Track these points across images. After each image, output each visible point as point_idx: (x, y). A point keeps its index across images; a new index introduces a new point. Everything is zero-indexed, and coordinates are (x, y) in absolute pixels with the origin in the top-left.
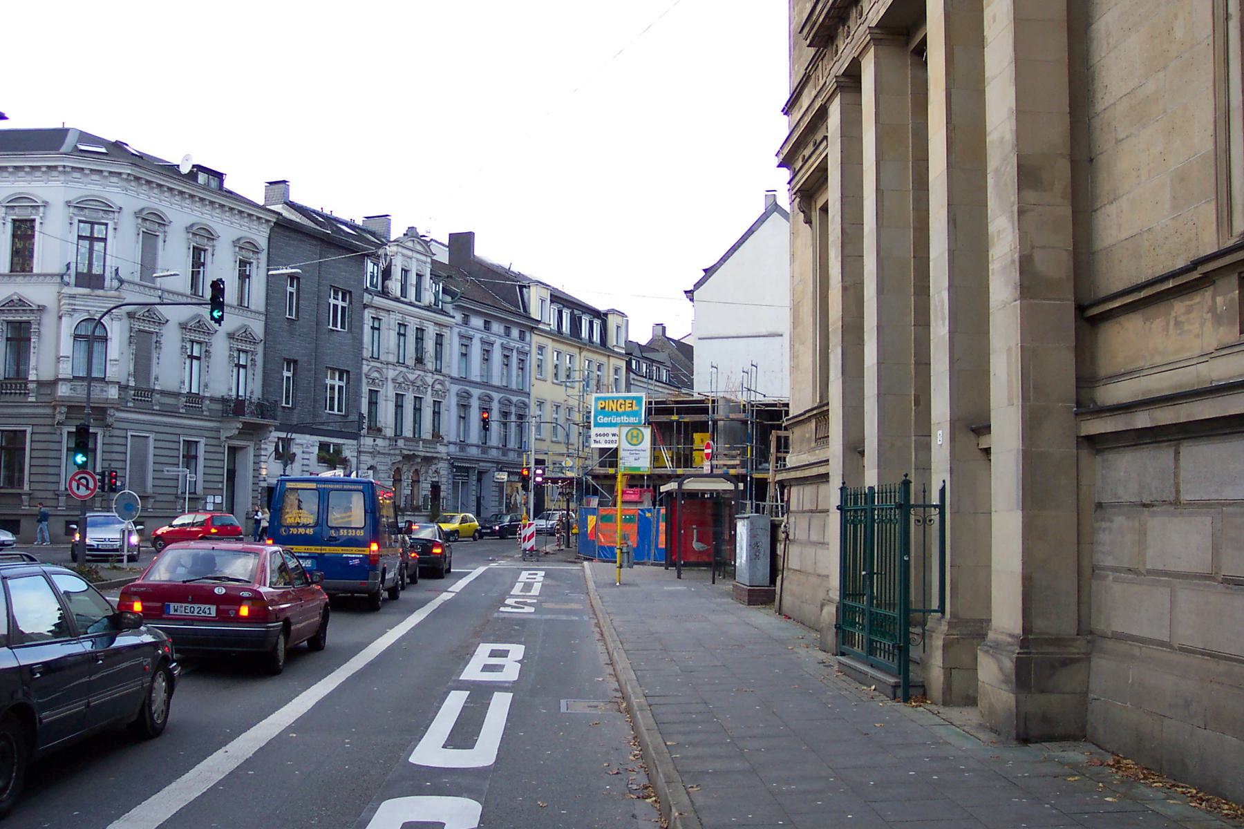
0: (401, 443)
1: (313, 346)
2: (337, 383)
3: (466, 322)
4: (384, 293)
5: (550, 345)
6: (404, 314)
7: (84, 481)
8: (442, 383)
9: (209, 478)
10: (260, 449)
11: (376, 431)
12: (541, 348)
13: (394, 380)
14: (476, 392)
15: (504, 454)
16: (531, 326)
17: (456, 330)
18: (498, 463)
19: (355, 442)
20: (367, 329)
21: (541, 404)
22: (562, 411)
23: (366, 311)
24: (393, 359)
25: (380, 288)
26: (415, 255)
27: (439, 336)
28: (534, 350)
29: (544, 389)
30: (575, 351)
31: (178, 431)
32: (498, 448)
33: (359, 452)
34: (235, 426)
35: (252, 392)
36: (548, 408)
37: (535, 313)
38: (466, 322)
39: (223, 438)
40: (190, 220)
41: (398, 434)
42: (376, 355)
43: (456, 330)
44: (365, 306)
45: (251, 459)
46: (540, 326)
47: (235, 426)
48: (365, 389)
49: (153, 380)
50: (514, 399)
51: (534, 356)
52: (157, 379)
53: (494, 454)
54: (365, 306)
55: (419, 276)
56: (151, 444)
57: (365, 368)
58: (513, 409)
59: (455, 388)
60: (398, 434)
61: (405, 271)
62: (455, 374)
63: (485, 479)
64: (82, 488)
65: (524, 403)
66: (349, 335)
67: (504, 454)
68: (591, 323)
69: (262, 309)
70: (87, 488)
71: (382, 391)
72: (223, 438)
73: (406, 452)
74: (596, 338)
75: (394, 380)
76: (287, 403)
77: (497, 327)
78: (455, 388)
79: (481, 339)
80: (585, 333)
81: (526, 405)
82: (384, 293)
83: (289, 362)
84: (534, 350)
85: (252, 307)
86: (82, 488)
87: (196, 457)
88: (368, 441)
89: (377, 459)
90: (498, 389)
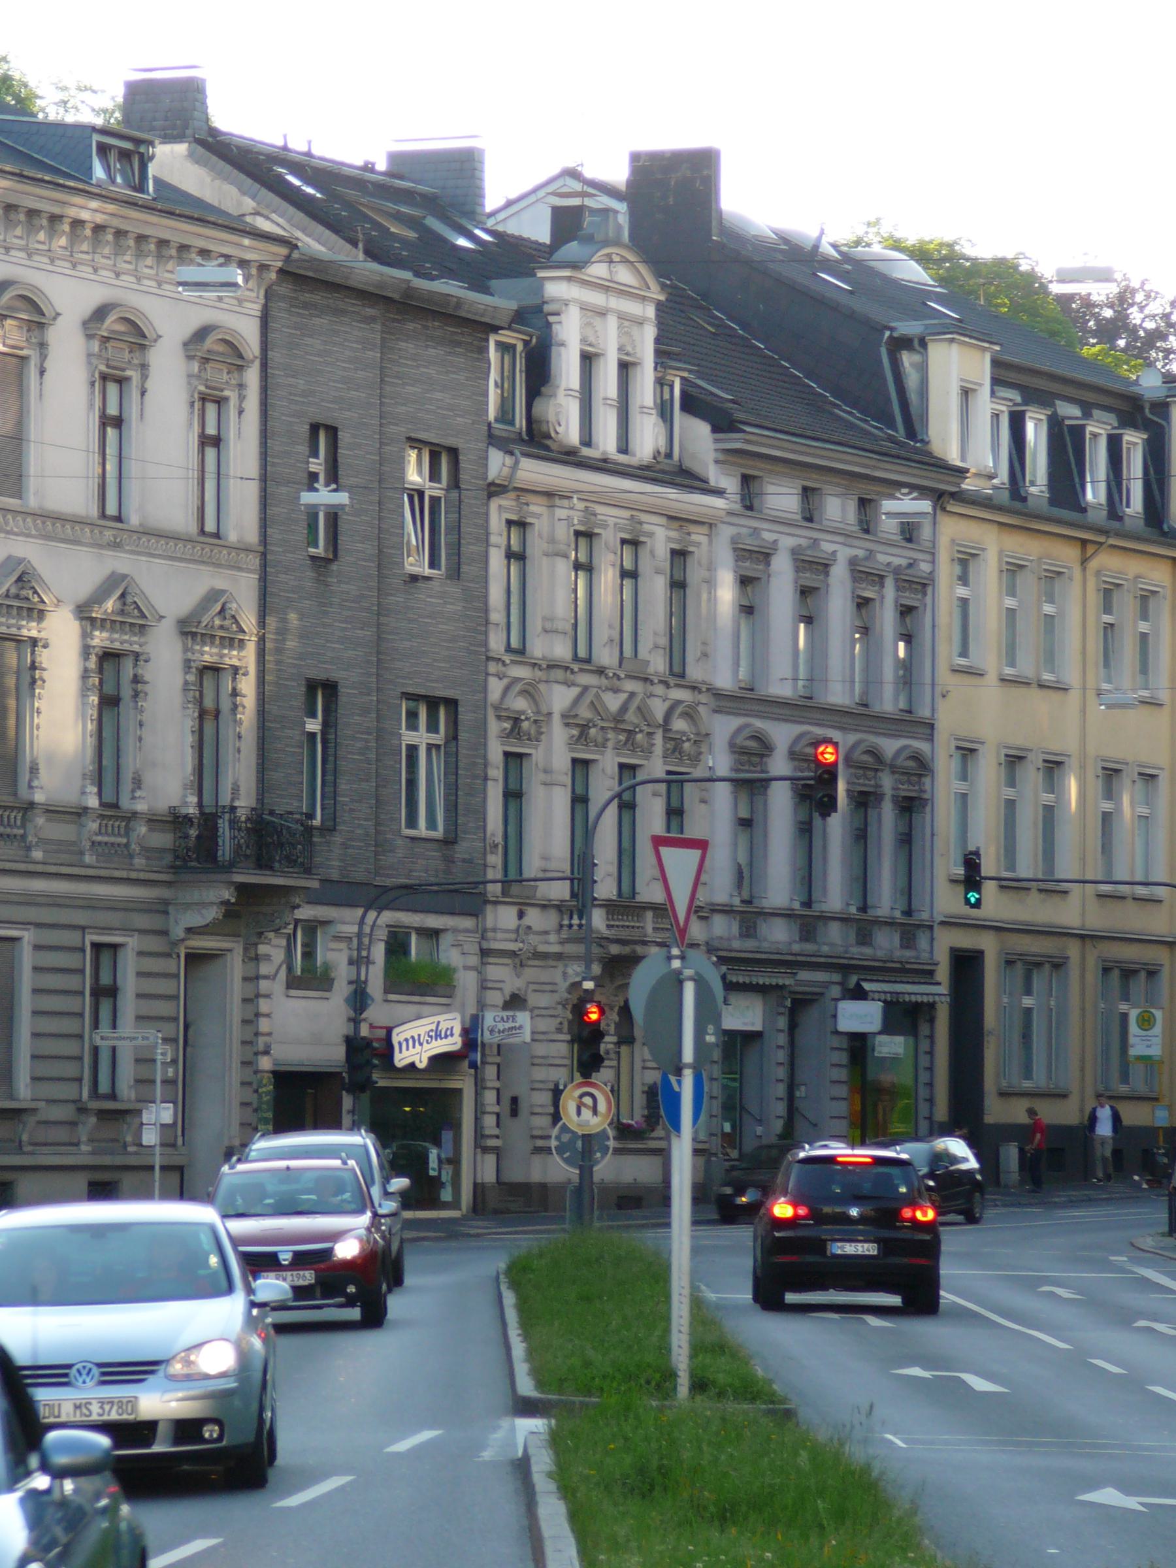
0: (598, 920)
1: (369, 633)
2: (421, 737)
3: (749, 501)
4: (536, 440)
5: (994, 545)
6: (592, 498)
7: (588, 1100)
8: (690, 714)
9: (51, 1047)
10: (257, 958)
11: (515, 882)
12: (966, 561)
13: (568, 718)
14: (782, 734)
15: (864, 938)
16: (945, 487)
17: (726, 533)
18: (845, 969)
19: (467, 923)
20: (496, 560)
21: (967, 752)
22: (1031, 775)
23: (494, 504)
24: (561, 650)
25: (520, 422)
26: (615, 303)
27: (679, 555)
28: (946, 571)
29: (975, 709)
30: (1068, 554)
31: (80, 918)
32: (845, 920)
33: (485, 953)
34: (208, 899)
35: (236, 790)
36: (988, 768)
37: (945, 440)
38: (749, 501)
39: (178, 932)
40: (95, 295)
41: (582, 896)
42: (582, 653)
43: (726, 533)
44: (495, 490)
45: (237, 989)
46: (968, 485)
47: (208, 899)
48: (495, 751)
49: (127, 785)
50: (890, 746)
51: (947, 590)
52: (138, 783)
53: (835, 938)
54: (495, 490)
55: (625, 367)
56: (27, 958)
57: (495, 688)
58: (887, 782)
59: (723, 728)
60: (582, 896)
61: (588, 359)
62: (724, 680)
63: (811, 1018)
64: (587, 1114)
65: (917, 757)
66: (454, 589)
67: (864, 938)
68: (1114, 443)
69: (252, 536)
70: (595, 1111)
71: (538, 755)
72: (178, 932)
73: (615, 949)
74: (1136, 504)
75: (568, 718)
76: (432, 824)
77: (782, 498)
78: (723, 728)
79: (795, 552)
80: (1094, 494)
81: (922, 767)
82: (536, 440)
83: (433, 703)
84: (946, 571)
85: (232, 537)
86: (587, 1114)
87: (112, 992)
88: (504, 917)
89: (530, 973)
90: (726, 702)
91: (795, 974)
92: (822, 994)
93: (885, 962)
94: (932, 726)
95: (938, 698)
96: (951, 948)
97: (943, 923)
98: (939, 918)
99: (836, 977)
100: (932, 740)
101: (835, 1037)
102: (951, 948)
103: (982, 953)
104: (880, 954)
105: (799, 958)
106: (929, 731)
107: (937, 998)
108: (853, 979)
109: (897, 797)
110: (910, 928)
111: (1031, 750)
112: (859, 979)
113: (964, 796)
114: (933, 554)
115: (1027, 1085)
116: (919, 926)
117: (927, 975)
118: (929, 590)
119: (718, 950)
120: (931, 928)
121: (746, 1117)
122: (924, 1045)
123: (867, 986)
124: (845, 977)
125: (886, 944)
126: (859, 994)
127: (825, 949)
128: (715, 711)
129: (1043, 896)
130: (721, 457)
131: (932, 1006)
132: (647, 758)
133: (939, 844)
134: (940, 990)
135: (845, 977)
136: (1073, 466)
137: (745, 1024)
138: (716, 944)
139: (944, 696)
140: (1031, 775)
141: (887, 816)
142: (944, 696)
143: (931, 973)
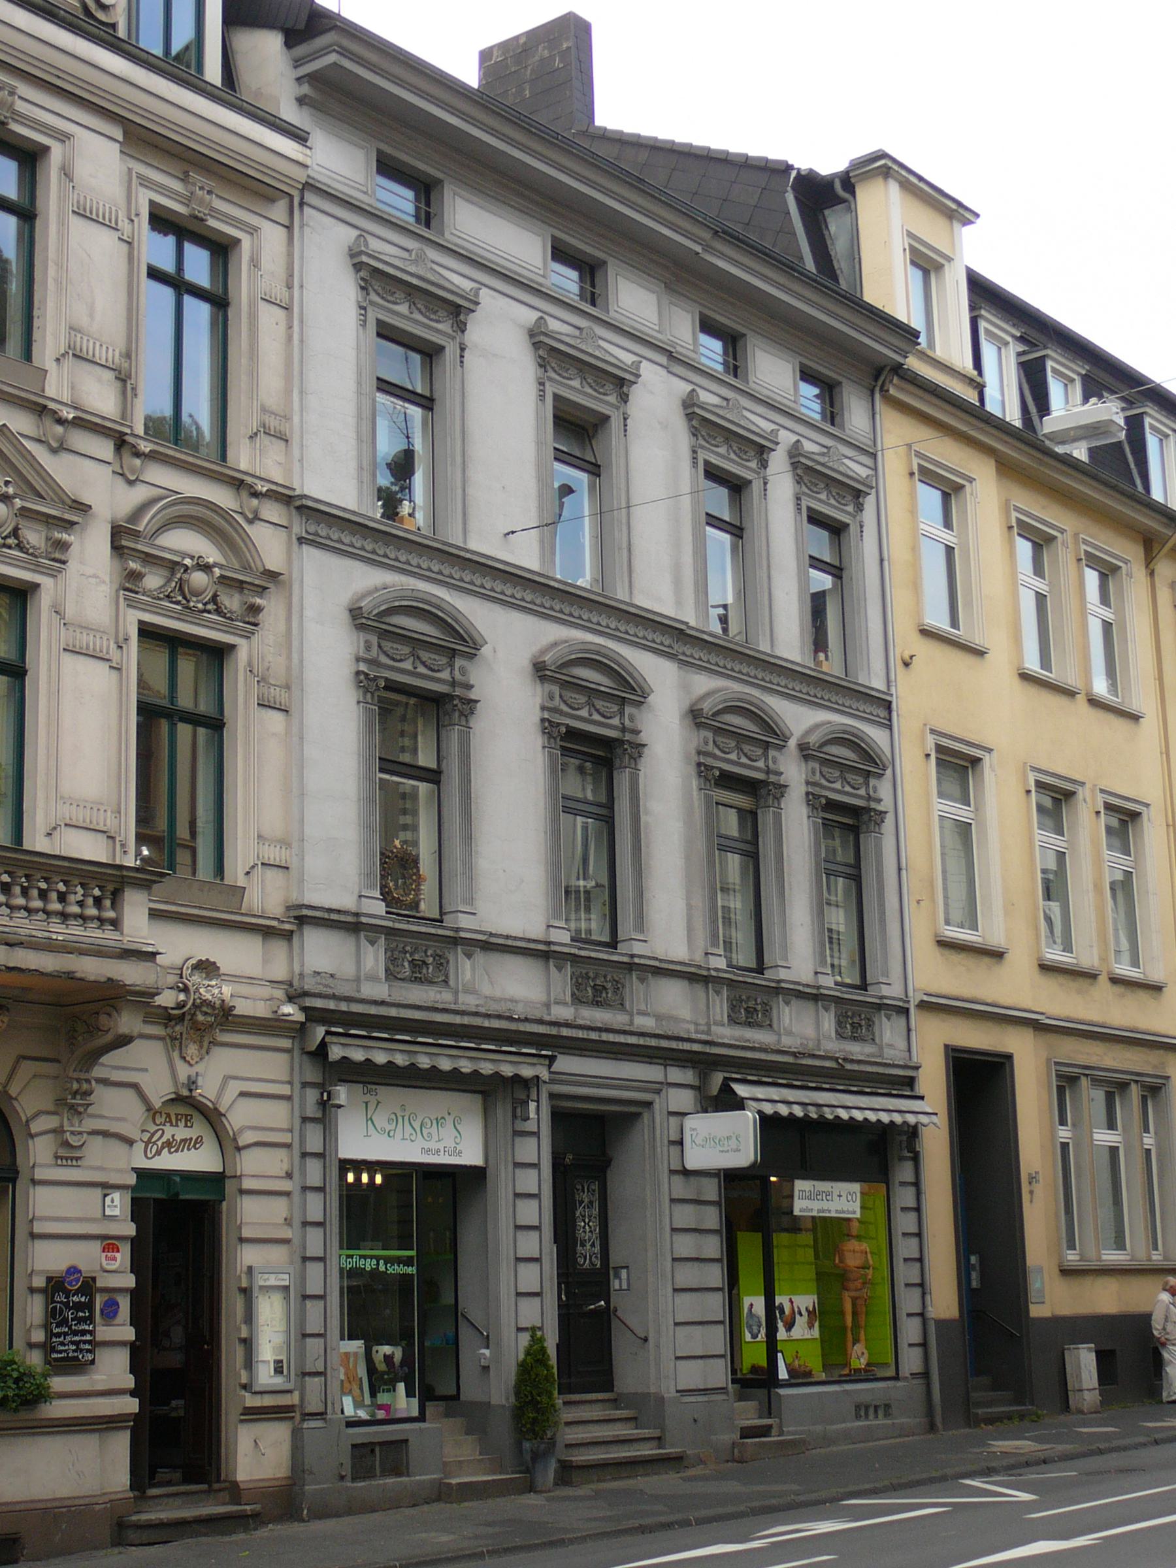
21: (958, 764)
22: (1088, 824)
91: (552, 1059)
92: (649, 1104)
93: (794, 1054)
94: (888, 706)
95: (899, 671)
96: (946, 1046)
97: (923, 1005)
98: (915, 998)
99: (687, 1076)
100: (890, 727)
101: (678, 1180)
102: (946, 1046)
103: (1009, 1057)
104: (787, 1042)
105: (565, 1032)
106: (883, 713)
107: (924, 1119)
108: (717, 1078)
109: (817, 797)
110: (858, 1010)
111: (1083, 784)
112: (725, 1078)
113: (964, 830)
114: (874, 456)
115: (1112, 1257)
116: (879, 1007)
117: (903, 1084)
118: (869, 502)
119: (306, 994)
120: (906, 1012)
121: (462, 1324)
122: (906, 1197)
123: (741, 1090)
124: (704, 1077)
125: (801, 1029)
126: (727, 1101)
127: (644, 1023)
128: (301, 540)
129: (1119, 989)
130: (306, 89)
131: (913, 1132)
132: (53, 574)
133: (913, 884)
134: (930, 1110)
135: (704, 1077)
136: (1132, 466)
137: (427, 1151)
138: (310, 985)
139: (907, 665)
140: (1088, 824)
141: (796, 829)
142: (907, 665)
143: (910, 1082)
